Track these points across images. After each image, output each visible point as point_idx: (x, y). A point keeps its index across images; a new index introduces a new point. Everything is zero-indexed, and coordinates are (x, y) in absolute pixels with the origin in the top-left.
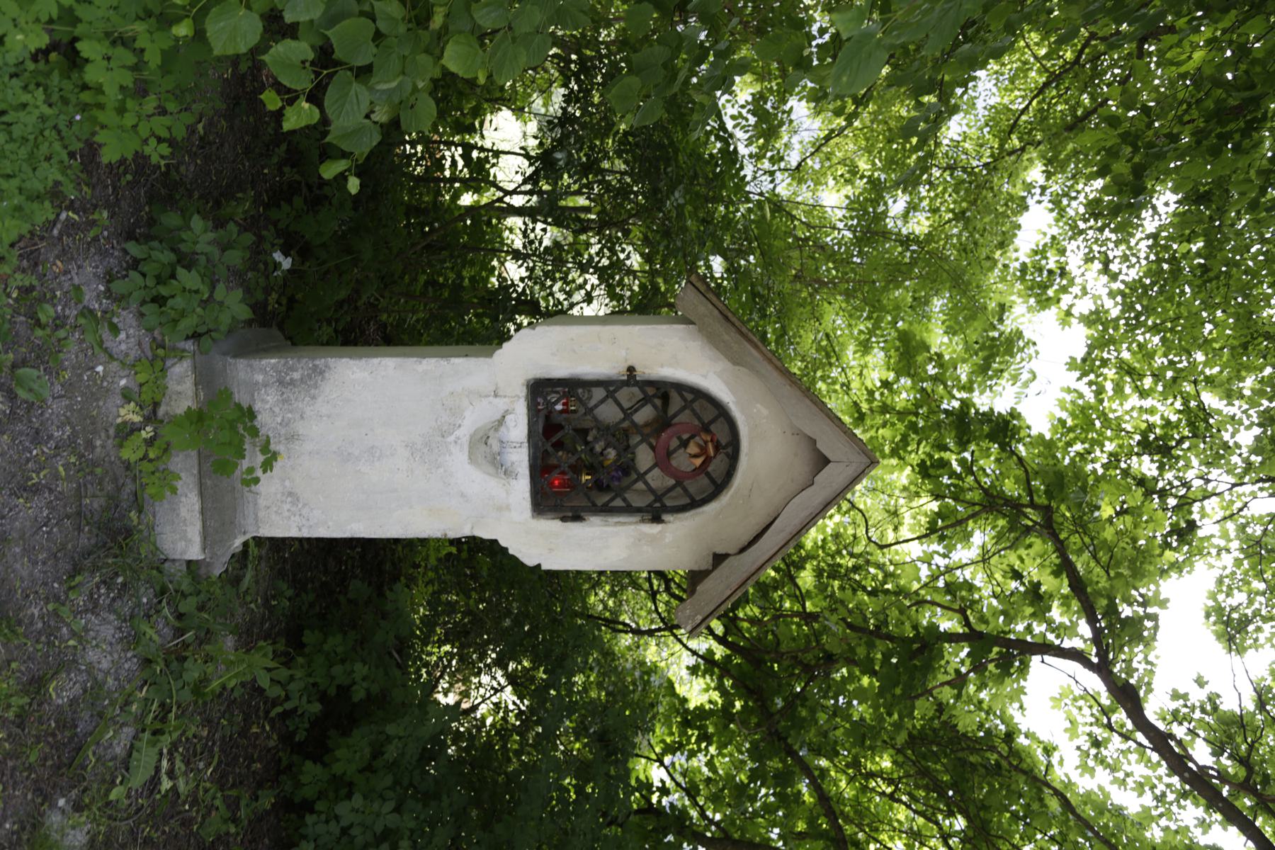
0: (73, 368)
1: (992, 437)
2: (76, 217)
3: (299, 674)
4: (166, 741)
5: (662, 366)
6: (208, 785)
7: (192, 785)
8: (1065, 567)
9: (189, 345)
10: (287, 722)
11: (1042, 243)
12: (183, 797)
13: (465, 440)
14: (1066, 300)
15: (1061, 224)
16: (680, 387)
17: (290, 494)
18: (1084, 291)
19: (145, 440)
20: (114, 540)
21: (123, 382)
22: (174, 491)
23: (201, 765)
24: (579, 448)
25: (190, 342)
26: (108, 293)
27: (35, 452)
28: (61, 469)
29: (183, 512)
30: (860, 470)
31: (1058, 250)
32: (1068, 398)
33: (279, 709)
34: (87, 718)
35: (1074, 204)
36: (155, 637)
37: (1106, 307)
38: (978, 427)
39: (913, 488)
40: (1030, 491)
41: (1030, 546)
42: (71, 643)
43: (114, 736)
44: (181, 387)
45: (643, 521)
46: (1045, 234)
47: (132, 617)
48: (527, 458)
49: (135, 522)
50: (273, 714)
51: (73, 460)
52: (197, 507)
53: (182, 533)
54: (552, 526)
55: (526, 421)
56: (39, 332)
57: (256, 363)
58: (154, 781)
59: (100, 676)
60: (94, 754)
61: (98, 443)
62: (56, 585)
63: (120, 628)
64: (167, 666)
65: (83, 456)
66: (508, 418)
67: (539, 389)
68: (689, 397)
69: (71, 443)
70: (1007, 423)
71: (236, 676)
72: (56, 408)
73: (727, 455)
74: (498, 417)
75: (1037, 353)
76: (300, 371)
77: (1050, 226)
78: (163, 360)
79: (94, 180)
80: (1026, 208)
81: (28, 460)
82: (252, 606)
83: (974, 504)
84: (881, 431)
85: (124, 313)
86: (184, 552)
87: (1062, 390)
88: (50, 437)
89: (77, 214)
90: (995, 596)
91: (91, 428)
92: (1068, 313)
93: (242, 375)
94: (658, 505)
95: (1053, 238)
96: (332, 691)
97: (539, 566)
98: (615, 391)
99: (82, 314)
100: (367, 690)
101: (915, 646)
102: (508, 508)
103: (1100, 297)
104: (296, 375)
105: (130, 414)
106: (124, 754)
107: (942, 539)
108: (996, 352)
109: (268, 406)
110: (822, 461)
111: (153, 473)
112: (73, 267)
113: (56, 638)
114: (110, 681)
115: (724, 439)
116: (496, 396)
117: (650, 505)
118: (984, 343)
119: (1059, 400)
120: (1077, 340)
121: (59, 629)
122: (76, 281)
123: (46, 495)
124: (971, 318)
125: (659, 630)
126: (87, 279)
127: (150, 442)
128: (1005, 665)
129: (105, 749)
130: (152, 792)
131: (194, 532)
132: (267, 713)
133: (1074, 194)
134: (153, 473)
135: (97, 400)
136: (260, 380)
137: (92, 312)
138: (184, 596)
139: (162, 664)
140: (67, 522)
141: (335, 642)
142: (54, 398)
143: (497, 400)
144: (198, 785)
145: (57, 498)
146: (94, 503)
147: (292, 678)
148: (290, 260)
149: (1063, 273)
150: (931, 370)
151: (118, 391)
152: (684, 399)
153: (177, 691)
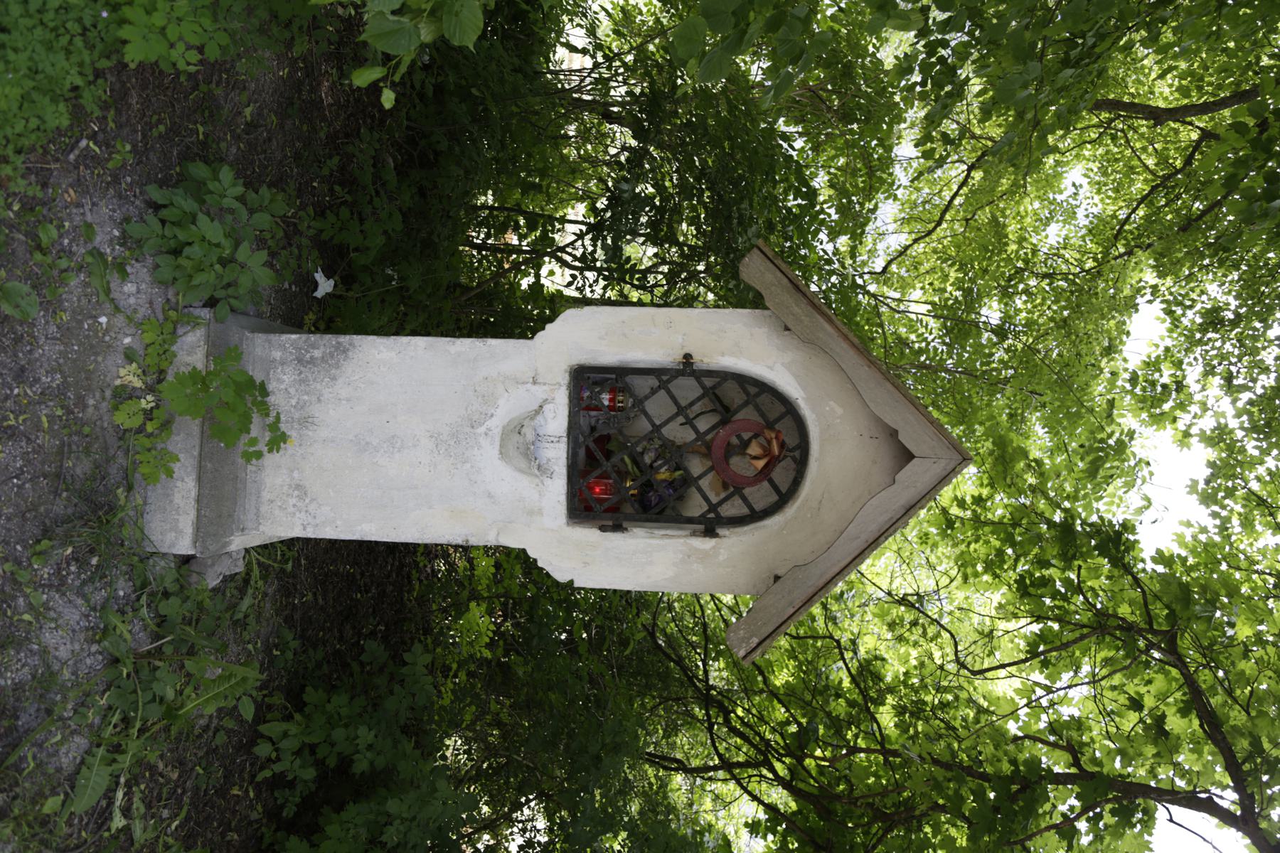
0: (74, 312)
1: (1103, 550)
2: (97, 149)
3: (293, 729)
4: (126, 761)
5: (723, 355)
6: (170, 840)
7: (151, 835)
8: (1195, 702)
9: (206, 313)
10: (276, 794)
11: (1153, 356)
12: (137, 845)
13: (497, 432)
14: (1184, 419)
15: (1175, 335)
16: (742, 380)
17: (298, 487)
18: (1204, 407)
19: (144, 410)
20: (94, 512)
21: (127, 340)
22: (170, 474)
23: (166, 813)
24: (625, 454)
25: (206, 310)
26: (124, 240)
27: (16, 391)
28: (44, 419)
29: (177, 499)
30: (949, 468)
31: (1172, 362)
32: (1188, 533)
33: (267, 773)
34: (32, 711)
35: (1190, 313)
36: (127, 636)
37: (1231, 426)
38: (1085, 541)
39: (1011, 608)
40: (1149, 618)
41: (1149, 682)
42: (27, 617)
43: (61, 743)
44: (192, 351)
45: (694, 534)
46: (1157, 346)
47: (103, 607)
48: (565, 455)
49: (122, 502)
50: (259, 778)
51: (59, 412)
52: (194, 493)
53: (173, 525)
54: (589, 535)
55: (566, 413)
56: (38, 256)
57: (274, 338)
58: (102, 816)
59: (56, 667)
60: (34, 758)
61: (91, 402)
62: (19, 547)
63: (87, 616)
64: (137, 672)
65: (73, 413)
66: (547, 407)
67: (588, 381)
68: (753, 390)
69: (61, 391)
70: (1119, 534)
71: (215, 697)
72: (48, 351)
73: (794, 458)
74: (536, 407)
75: (1151, 474)
76: (322, 349)
77: (1162, 339)
78: (175, 323)
79: (124, 119)
80: (1135, 307)
81: (7, 398)
82: (250, 647)
83: (1083, 626)
84: (973, 546)
85: (137, 265)
86: (173, 545)
87: (1181, 523)
88: (37, 380)
89: (100, 148)
90: (1108, 736)
91: (85, 383)
92: (1187, 434)
93: (259, 351)
94: (712, 515)
95: (1167, 349)
96: (332, 762)
97: (572, 582)
98: (669, 381)
99: (90, 253)
100: (372, 763)
101: (1015, 788)
102: (540, 512)
103: (1223, 415)
104: (317, 353)
105: (130, 376)
106: (71, 769)
107: (1045, 664)
108: (1104, 458)
109: (282, 387)
110: (906, 456)
111: (149, 450)
112: (87, 201)
113: (9, 606)
114: (66, 674)
115: (792, 441)
116: (535, 383)
117: (703, 515)
118: (1091, 446)
119: (1176, 534)
120: (1198, 460)
121: (14, 598)
122: (89, 218)
123: (23, 444)
124: (1074, 419)
125: (715, 768)
126: (103, 221)
127: (149, 415)
128: (1125, 815)
129: (49, 755)
130: (100, 827)
131: (187, 523)
132: (254, 776)
133: (1188, 303)
134: (149, 450)
135: (96, 354)
136: (278, 357)
137: (102, 255)
138: (166, 595)
139: (131, 668)
140: (43, 482)
141: (340, 702)
142: (47, 338)
143: (536, 387)
144: (158, 837)
145: (34, 451)
146: (80, 467)
147: (285, 735)
148: (332, 282)
149: (1180, 386)
150: (1031, 480)
151: (121, 349)
152: (748, 394)
153: (144, 704)
